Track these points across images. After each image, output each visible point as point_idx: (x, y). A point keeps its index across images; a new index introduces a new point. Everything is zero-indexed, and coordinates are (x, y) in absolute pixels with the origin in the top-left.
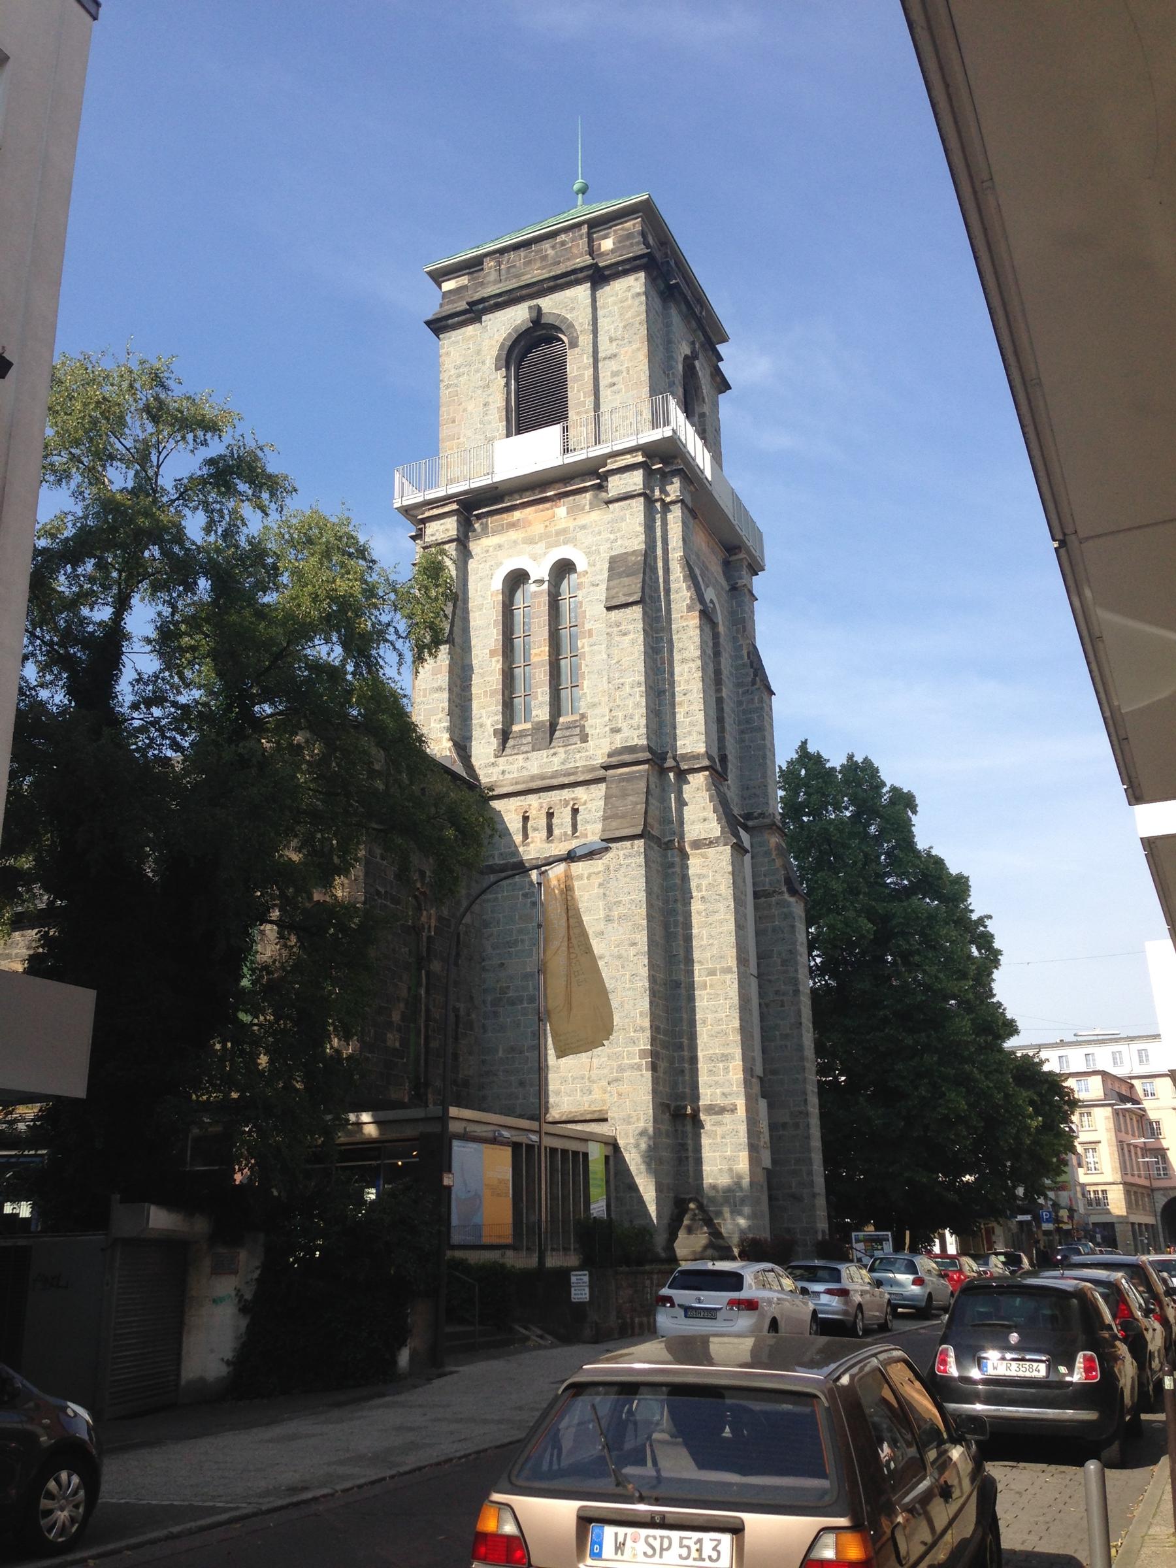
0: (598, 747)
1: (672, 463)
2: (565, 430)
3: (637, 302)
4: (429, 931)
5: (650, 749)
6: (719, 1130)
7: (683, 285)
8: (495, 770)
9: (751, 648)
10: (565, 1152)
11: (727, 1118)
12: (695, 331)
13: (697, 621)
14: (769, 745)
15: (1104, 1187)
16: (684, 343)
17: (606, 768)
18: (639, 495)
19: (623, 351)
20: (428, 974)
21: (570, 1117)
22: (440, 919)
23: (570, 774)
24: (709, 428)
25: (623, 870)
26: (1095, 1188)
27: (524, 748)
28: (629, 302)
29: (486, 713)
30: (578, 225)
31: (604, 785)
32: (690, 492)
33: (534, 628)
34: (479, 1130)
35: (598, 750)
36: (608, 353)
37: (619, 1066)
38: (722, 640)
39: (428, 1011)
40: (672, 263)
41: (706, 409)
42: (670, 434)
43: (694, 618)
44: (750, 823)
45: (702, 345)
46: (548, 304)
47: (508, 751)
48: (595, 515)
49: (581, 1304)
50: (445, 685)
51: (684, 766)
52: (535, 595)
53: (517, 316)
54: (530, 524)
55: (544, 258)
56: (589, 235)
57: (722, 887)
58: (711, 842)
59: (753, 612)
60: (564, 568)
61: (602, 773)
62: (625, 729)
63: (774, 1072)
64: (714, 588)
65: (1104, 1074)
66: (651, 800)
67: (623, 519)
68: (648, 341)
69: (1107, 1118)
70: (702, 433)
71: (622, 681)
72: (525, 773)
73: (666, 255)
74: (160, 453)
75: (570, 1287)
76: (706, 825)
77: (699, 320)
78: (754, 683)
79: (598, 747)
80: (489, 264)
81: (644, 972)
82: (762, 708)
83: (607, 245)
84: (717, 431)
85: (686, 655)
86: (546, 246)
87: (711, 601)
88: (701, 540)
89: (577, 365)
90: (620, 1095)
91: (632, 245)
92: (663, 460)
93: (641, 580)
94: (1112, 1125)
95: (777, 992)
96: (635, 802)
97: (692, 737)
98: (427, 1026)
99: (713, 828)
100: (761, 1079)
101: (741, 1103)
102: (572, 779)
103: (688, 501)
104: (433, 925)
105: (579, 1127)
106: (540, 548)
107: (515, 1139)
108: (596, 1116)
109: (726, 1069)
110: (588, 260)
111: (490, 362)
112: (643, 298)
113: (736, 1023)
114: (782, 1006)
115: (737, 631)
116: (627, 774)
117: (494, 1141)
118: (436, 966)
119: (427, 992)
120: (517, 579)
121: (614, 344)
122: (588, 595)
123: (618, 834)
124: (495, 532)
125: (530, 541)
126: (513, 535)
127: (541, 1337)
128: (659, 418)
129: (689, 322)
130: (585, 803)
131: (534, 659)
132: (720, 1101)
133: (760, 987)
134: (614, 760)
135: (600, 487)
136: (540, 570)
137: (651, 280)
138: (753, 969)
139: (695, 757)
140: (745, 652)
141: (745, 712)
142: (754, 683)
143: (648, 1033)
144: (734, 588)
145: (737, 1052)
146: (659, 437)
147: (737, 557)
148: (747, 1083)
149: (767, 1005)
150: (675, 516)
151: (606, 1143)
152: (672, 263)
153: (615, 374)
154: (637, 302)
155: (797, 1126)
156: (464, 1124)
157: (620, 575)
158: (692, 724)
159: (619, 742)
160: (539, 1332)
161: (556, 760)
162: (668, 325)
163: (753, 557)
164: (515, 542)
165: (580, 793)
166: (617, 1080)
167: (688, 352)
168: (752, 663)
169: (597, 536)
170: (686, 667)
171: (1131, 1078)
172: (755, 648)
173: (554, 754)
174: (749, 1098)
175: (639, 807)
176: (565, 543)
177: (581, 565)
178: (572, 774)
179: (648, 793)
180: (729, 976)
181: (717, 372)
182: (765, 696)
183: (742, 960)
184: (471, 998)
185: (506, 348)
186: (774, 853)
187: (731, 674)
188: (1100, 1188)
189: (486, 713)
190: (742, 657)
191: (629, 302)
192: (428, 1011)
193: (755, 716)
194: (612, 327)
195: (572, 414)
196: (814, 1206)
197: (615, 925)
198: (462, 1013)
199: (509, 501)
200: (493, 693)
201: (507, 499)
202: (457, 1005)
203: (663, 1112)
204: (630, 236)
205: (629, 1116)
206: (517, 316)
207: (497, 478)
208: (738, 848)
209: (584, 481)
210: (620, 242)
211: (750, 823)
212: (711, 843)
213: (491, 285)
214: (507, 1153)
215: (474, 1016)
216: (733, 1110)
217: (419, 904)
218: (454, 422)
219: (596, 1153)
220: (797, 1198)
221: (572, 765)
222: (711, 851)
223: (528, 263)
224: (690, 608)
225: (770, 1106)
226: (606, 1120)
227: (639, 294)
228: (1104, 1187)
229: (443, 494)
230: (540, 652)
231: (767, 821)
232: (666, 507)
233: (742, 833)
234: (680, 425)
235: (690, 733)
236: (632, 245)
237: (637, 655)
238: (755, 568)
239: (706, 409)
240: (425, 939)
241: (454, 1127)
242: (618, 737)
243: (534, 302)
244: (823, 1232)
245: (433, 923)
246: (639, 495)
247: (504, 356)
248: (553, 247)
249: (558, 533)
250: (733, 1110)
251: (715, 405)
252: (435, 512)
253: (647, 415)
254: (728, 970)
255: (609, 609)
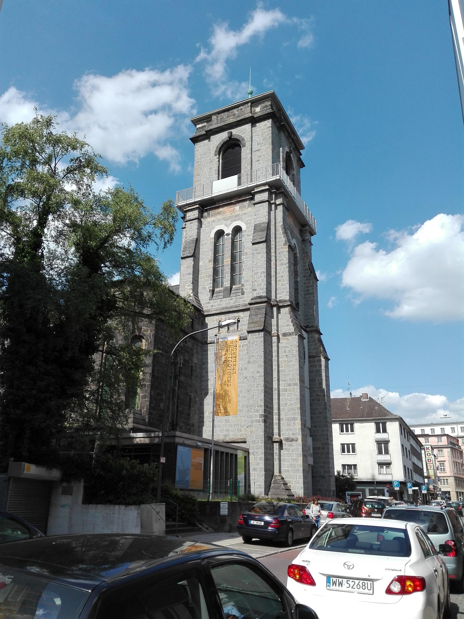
0: (248, 297)
1: (280, 190)
2: (239, 178)
3: (268, 130)
4: (180, 365)
5: (267, 297)
6: (291, 448)
7: (287, 126)
8: (209, 305)
9: (310, 263)
10: (227, 454)
11: (294, 443)
12: (291, 143)
13: (287, 249)
14: (316, 300)
15: (447, 478)
16: (286, 147)
17: (250, 304)
18: (266, 201)
19: (262, 148)
20: (179, 381)
21: (233, 440)
22: (185, 360)
23: (237, 307)
24: (296, 180)
25: (255, 343)
26: (443, 478)
27: (220, 297)
28: (265, 130)
29: (205, 282)
30: (247, 103)
31: (249, 312)
32: (287, 201)
33: (225, 252)
34: (187, 442)
35: (247, 298)
36: (257, 149)
37: (251, 420)
38: (298, 259)
39: (178, 396)
40: (283, 117)
41: (295, 172)
42: (279, 178)
43: (286, 248)
44: (308, 329)
45: (294, 149)
46: (235, 131)
47: (214, 298)
48: (250, 209)
49: (224, 516)
50: (191, 272)
51: (281, 304)
52: (227, 241)
53: (224, 136)
54: (225, 213)
55: (234, 115)
56: (251, 106)
57: (294, 351)
58: (290, 334)
59: (311, 249)
60: (237, 230)
61: (249, 306)
62: (258, 289)
63: (315, 427)
64: (296, 239)
65: (447, 436)
66: (267, 317)
67: (260, 210)
68: (272, 144)
69: (448, 452)
70: (293, 181)
71: (257, 271)
72: (220, 306)
73: (280, 114)
74: (56, 159)
75: (220, 508)
76: (288, 327)
77: (293, 140)
78: (310, 276)
79: (248, 297)
80: (214, 117)
81: (262, 383)
82: (313, 286)
83: (258, 109)
84: (299, 182)
85: (282, 262)
86: (235, 111)
87: (294, 244)
88: (290, 221)
89: (245, 153)
90: (251, 432)
91: (267, 109)
92: (276, 188)
93: (266, 233)
94: (450, 455)
95: (317, 395)
96: (261, 318)
97: (283, 292)
98: (178, 402)
99: (291, 328)
100: (310, 429)
101: (300, 437)
102: (237, 309)
103: (285, 204)
104: (182, 362)
105: (236, 444)
106: (228, 222)
107: (206, 447)
108: (242, 440)
109: (294, 423)
110: (250, 115)
111: (213, 152)
112: (271, 128)
113: (299, 406)
114: (319, 401)
115: (305, 256)
116: (258, 306)
117: (197, 447)
118: (182, 378)
119: (178, 388)
120: (220, 234)
121: (259, 145)
122: (246, 239)
123: (253, 329)
124: (212, 216)
125: (226, 219)
126: (219, 217)
127: (207, 529)
128: (275, 172)
129: (289, 140)
130: (242, 318)
131: (225, 263)
132: (292, 437)
133: (310, 393)
134: (253, 301)
135: (253, 199)
136: (228, 230)
137: (274, 122)
138: (307, 384)
139: (285, 301)
140: (307, 264)
141: (307, 287)
142: (310, 276)
143: (263, 408)
144: (304, 240)
145: (299, 417)
146: (274, 179)
147: (305, 228)
148: (303, 430)
149: (313, 400)
150: (280, 208)
151: (245, 451)
152: (283, 117)
153: (260, 156)
154: (268, 130)
155: (324, 448)
156: (184, 439)
157: (258, 231)
158: (284, 288)
159: (255, 294)
160: (206, 526)
161: (232, 301)
162: (280, 140)
163: (312, 229)
164: (220, 219)
165: (241, 314)
166: (250, 426)
167: (288, 150)
168: (310, 268)
169: (249, 217)
170: (282, 267)
171: (458, 437)
172: (311, 263)
173: (232, 299)
174: (303, 435)
175: (262, 319)
176: (238, 220)
177: (244, 228)
178: (238, 307)
179: (266, 314)
180: (296, 387)
181: (299, 160)
182: (315, 281)
183: (302, 380)
184: (196, 392)
185: (219, 147)
186: (317, 341)
187: (302, 272)
188: (445, 478)
189: (205, 282)
190: (306, 266)
191: (265, 130)
192: (178, 396)
193: (310, 288)
194: (258, 141)
195: (242, 171)
196: (330, 480)
197: (252, 365)
198: (192, 398)
199: (218, 204)
200: (209, 276)
201: (217, 203)
202: (191, 394)
203: (269, 440)
204: (266, 106)
205: (255, 441)
206: (224, 136)
207: (213, 196)
208: (301, 338)
209: (246, 196)
210: (263, 108)
211: (308, 329)
212: (290, 334)
213: (214, 125)
214: (202, 453)
215: (197, 399)
216: (297, 440)
217: (177, 354)
218: (199, 175)
219: (240, 455)
220: (323, 477)
221: (238, 303)
222: (290, 338)
223: (228, 117)
224: (285, 244)
225: (313, 440)
226: (245, 442)
227: (269, 127)
228: (447, 478)
229: (193, 201)
230: (227, 261)
231: (314, 328)
232: (276, 206)
233: (303, 331)
234: (282, 175)
235: (283, 292)
236: (267, 109)
237: (263, 262)
238: (312, 233)
239: (295, 172)
240: (178, 368)
241: (178, 440)
242: (255, 292)
243: (230, 131)
244: (334, 491)
245: (182, 361)
246: (266, 201)
247: (218, 150)
248: (238, 111)
249: (235, 216)
250: (297, 440)
251: (299, 172)
252: (190, 208)
253: (271, 172)
254: (296, 384)
255: (253, 244)
